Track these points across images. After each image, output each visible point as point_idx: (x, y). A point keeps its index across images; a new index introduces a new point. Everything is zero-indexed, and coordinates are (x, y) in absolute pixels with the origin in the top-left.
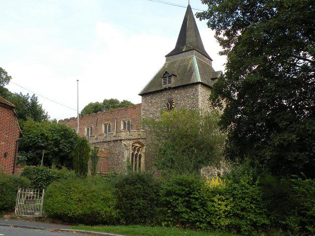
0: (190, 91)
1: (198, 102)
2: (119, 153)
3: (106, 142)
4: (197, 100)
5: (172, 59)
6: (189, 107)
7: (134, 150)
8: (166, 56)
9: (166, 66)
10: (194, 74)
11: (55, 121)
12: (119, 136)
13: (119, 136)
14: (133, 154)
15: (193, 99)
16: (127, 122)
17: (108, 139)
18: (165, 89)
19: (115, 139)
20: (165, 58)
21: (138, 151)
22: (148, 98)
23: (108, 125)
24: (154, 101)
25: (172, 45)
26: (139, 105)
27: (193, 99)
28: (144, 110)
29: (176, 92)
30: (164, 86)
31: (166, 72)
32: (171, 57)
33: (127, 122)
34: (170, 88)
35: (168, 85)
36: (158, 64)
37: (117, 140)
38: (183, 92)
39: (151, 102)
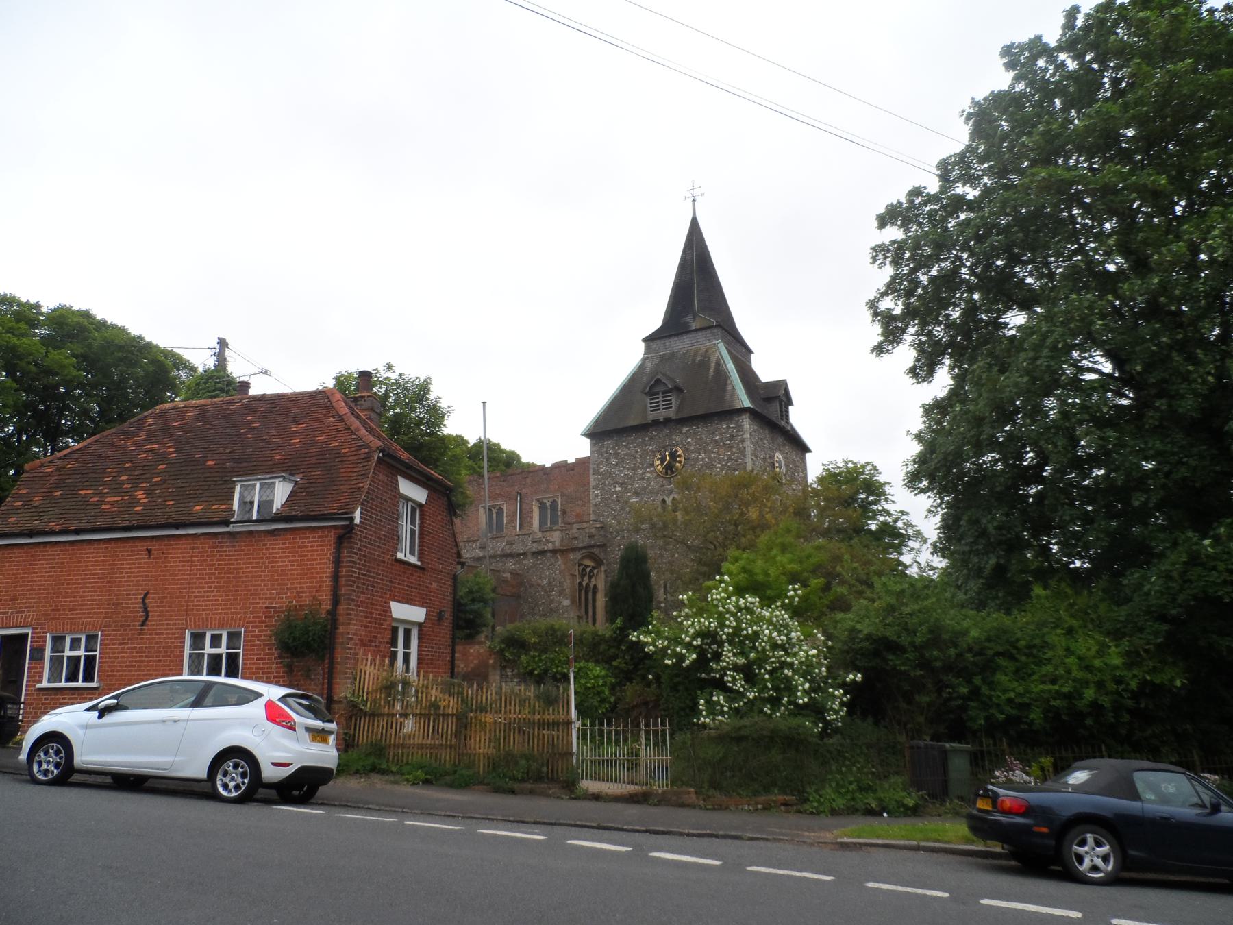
0: (724, 428)
1: (744, 456)
2: (549, 583)
3: (511, 555)
4: (743, 451)
5: (656, 345)
6: (722, 469)
7: (582, 576)
8: (645, 340)
9: (648, 364)
10: (730, 387)
11: (985, 99)
12: (548, 541)
13: (548, 541)
14: (580, 584)
15: (730, 448)
16: (548, 504)
17: (516, 548)
18: (656, 424)
19: (535, 547)
20: (642, 346)
21: (590, 578)
22: (630, 447)
23: (494, 511)
24: (623, 452)
25: (655, 320)
26: (581, 462)
27: (730, 448)
28: (596, 472)
29: (684, 430)
30: (652, 416)
31: (658, 381)
32: (658, 342)
33: (548, 504)
34: (667, 421)
35: (662, 414)
36: (622, 357)
37: (543, 552)
38: (702, 431)
39: (617, 455)
